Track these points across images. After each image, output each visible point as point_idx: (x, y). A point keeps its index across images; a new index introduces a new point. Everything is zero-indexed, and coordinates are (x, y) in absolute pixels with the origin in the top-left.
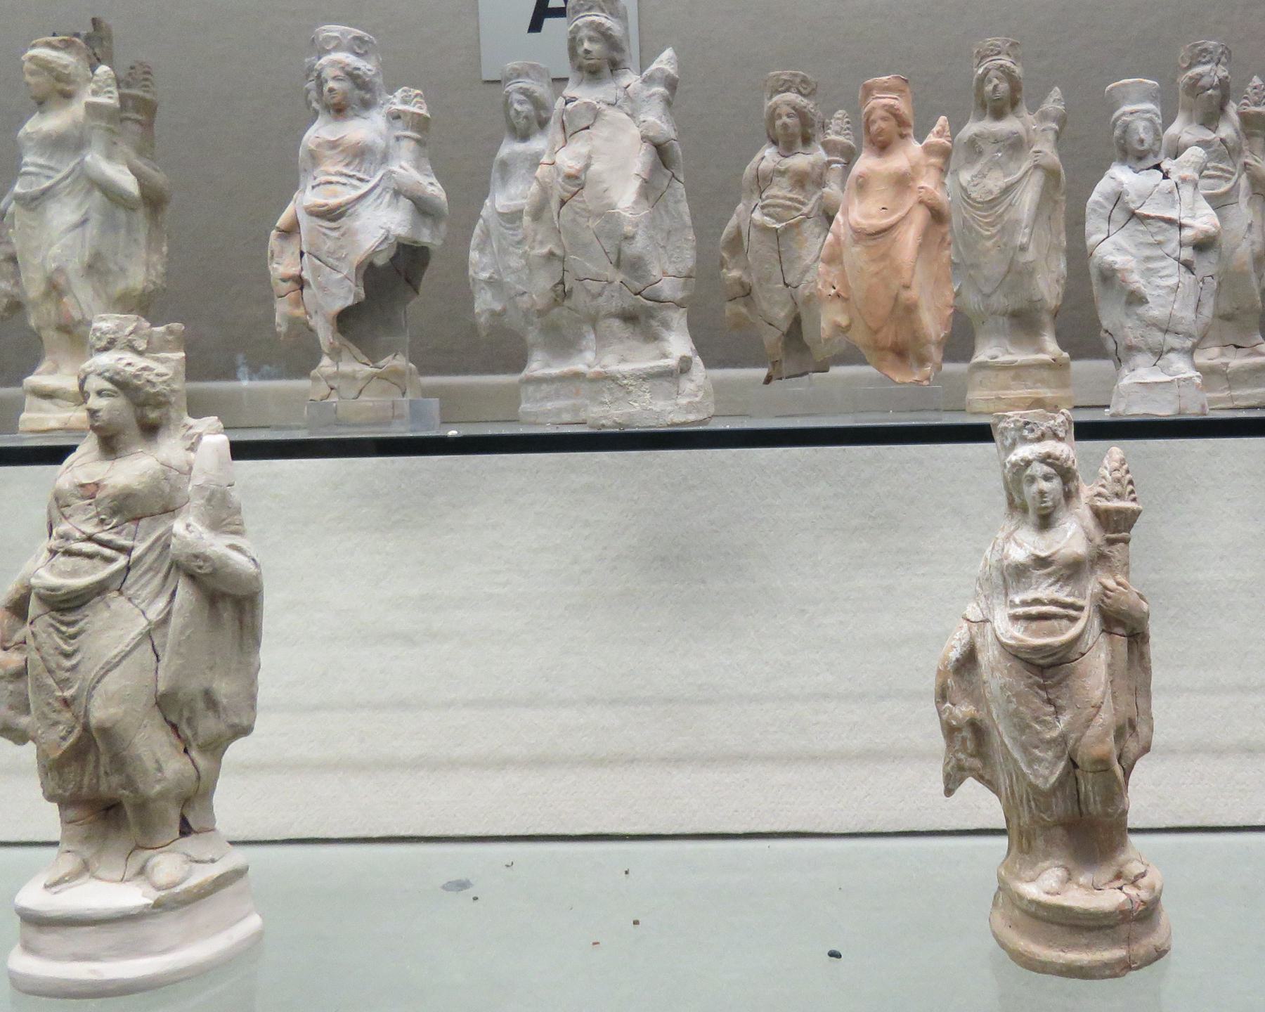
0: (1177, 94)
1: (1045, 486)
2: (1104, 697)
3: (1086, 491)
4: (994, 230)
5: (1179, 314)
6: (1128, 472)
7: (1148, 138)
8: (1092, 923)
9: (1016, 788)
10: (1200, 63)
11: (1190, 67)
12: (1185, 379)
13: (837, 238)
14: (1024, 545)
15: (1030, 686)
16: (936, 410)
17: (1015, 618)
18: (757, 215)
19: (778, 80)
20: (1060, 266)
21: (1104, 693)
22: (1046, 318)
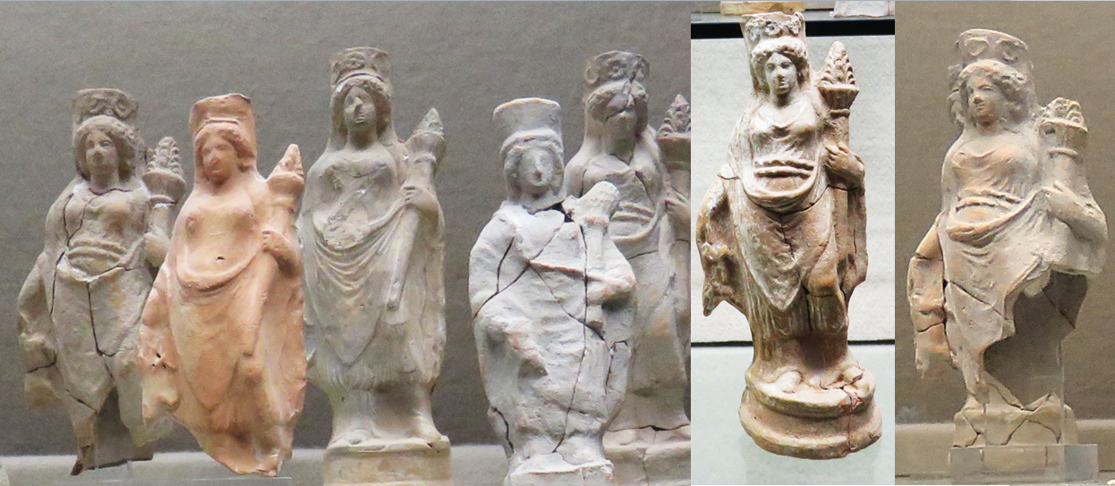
0: (583, 117)
1: (783, 72)
2: (829, 238)
3: (815, 76)
4: (356, 285)
5: (585, 389)
6: (848, 61)
7: (547, 172)
8: (819, 415)
9: (759, 309)
10: (610, 78)
11: (598, 84)
12: (592, 469)
13: (163, 295)
14: (768, 117)
15: (771, 229)
16: (697, 12)
17: (760, 176)
18: (64, 267)
19: (89, 100)
20: (438, 328)
21: (829, 235)
22: (420, 393)
